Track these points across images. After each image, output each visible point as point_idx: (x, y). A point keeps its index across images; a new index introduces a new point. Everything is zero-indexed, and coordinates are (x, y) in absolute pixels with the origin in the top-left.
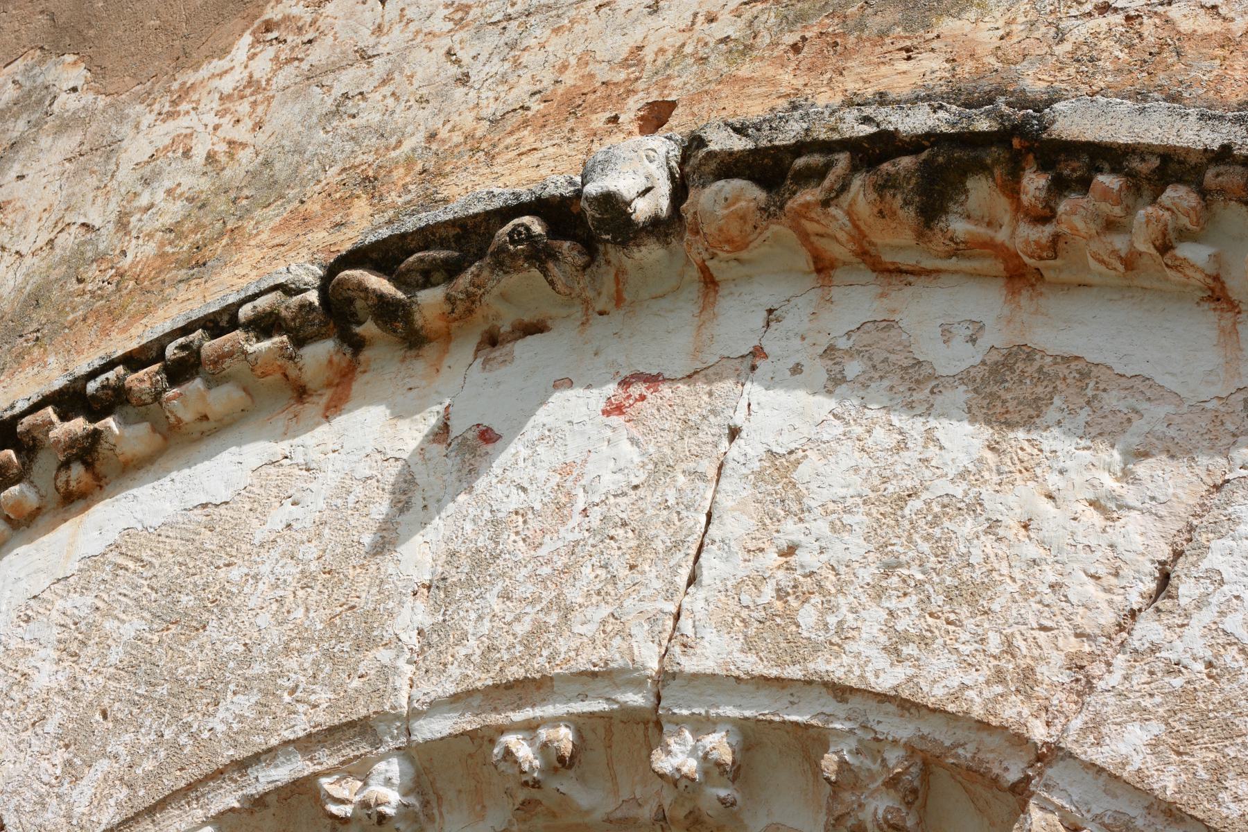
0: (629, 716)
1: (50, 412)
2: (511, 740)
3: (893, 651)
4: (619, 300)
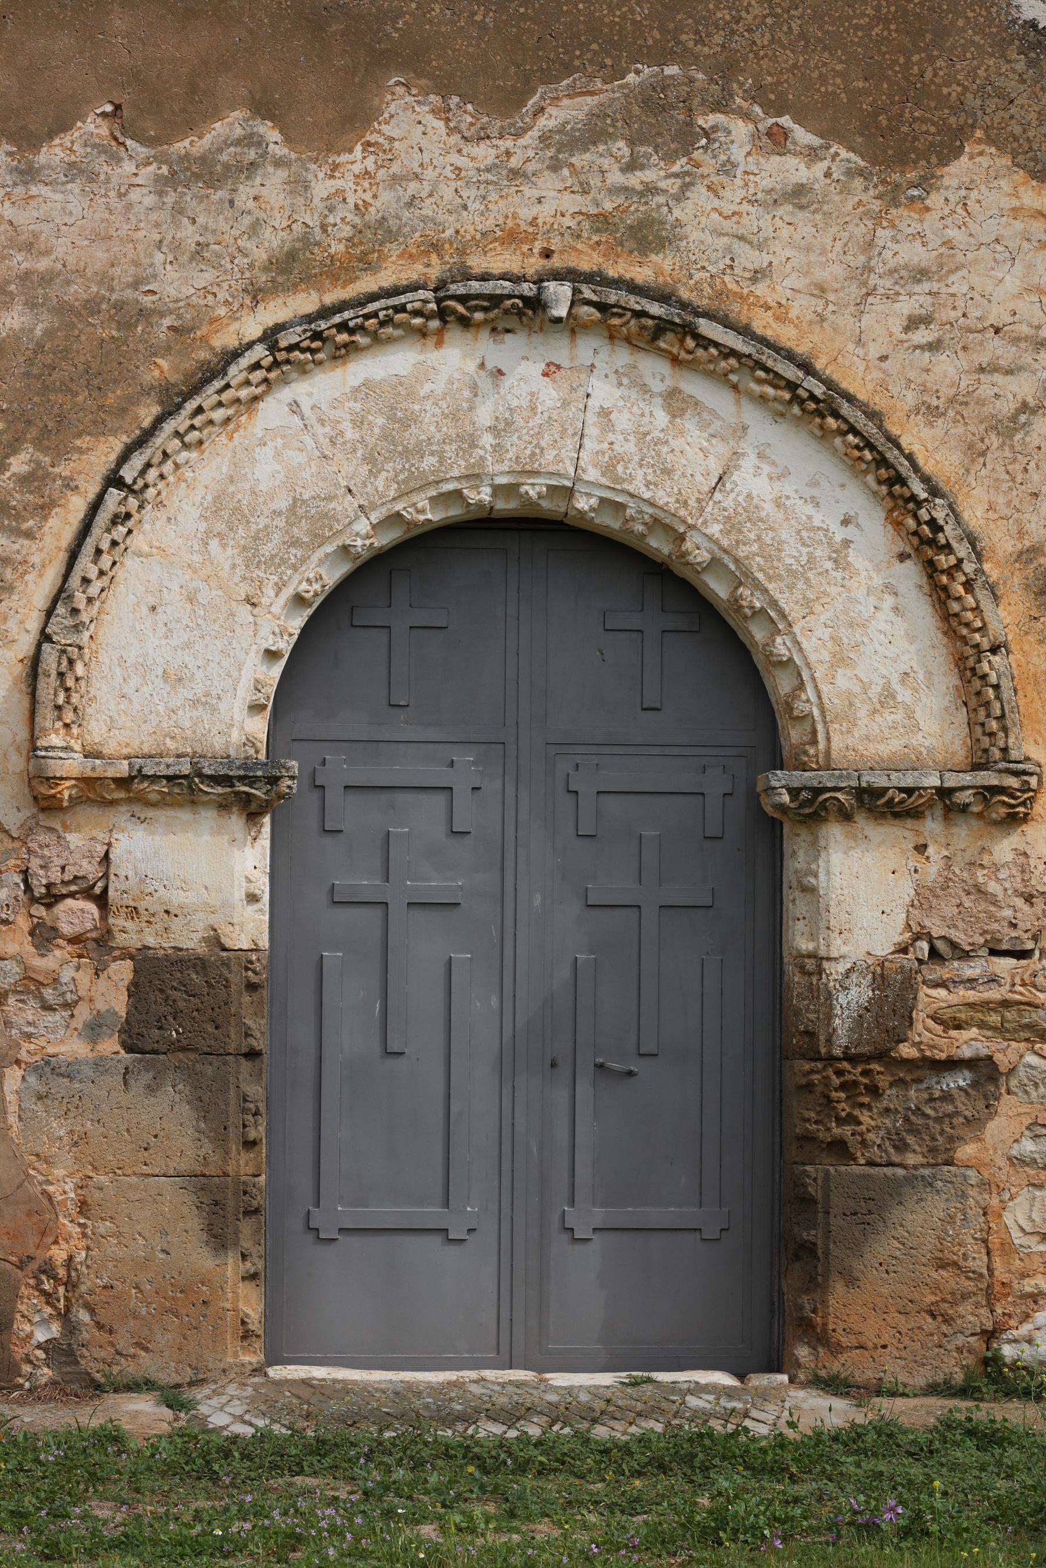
0: (564, 488)
1: (334, 330)
2: (527, 487)
3: (647, 486)
4: (541, 329)
